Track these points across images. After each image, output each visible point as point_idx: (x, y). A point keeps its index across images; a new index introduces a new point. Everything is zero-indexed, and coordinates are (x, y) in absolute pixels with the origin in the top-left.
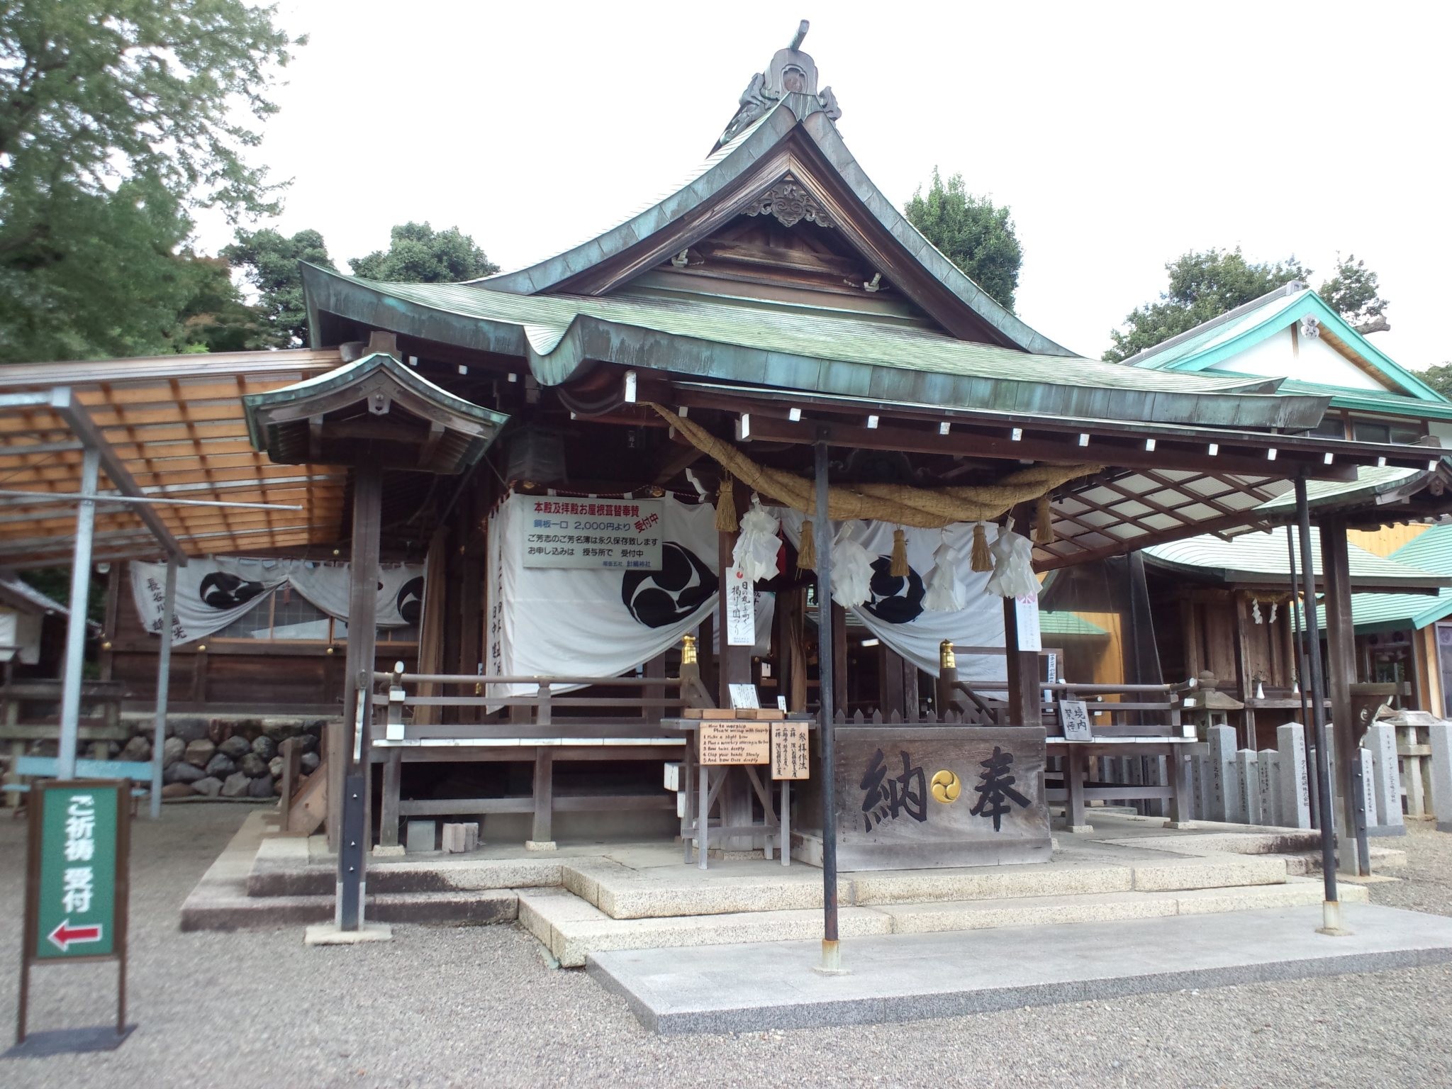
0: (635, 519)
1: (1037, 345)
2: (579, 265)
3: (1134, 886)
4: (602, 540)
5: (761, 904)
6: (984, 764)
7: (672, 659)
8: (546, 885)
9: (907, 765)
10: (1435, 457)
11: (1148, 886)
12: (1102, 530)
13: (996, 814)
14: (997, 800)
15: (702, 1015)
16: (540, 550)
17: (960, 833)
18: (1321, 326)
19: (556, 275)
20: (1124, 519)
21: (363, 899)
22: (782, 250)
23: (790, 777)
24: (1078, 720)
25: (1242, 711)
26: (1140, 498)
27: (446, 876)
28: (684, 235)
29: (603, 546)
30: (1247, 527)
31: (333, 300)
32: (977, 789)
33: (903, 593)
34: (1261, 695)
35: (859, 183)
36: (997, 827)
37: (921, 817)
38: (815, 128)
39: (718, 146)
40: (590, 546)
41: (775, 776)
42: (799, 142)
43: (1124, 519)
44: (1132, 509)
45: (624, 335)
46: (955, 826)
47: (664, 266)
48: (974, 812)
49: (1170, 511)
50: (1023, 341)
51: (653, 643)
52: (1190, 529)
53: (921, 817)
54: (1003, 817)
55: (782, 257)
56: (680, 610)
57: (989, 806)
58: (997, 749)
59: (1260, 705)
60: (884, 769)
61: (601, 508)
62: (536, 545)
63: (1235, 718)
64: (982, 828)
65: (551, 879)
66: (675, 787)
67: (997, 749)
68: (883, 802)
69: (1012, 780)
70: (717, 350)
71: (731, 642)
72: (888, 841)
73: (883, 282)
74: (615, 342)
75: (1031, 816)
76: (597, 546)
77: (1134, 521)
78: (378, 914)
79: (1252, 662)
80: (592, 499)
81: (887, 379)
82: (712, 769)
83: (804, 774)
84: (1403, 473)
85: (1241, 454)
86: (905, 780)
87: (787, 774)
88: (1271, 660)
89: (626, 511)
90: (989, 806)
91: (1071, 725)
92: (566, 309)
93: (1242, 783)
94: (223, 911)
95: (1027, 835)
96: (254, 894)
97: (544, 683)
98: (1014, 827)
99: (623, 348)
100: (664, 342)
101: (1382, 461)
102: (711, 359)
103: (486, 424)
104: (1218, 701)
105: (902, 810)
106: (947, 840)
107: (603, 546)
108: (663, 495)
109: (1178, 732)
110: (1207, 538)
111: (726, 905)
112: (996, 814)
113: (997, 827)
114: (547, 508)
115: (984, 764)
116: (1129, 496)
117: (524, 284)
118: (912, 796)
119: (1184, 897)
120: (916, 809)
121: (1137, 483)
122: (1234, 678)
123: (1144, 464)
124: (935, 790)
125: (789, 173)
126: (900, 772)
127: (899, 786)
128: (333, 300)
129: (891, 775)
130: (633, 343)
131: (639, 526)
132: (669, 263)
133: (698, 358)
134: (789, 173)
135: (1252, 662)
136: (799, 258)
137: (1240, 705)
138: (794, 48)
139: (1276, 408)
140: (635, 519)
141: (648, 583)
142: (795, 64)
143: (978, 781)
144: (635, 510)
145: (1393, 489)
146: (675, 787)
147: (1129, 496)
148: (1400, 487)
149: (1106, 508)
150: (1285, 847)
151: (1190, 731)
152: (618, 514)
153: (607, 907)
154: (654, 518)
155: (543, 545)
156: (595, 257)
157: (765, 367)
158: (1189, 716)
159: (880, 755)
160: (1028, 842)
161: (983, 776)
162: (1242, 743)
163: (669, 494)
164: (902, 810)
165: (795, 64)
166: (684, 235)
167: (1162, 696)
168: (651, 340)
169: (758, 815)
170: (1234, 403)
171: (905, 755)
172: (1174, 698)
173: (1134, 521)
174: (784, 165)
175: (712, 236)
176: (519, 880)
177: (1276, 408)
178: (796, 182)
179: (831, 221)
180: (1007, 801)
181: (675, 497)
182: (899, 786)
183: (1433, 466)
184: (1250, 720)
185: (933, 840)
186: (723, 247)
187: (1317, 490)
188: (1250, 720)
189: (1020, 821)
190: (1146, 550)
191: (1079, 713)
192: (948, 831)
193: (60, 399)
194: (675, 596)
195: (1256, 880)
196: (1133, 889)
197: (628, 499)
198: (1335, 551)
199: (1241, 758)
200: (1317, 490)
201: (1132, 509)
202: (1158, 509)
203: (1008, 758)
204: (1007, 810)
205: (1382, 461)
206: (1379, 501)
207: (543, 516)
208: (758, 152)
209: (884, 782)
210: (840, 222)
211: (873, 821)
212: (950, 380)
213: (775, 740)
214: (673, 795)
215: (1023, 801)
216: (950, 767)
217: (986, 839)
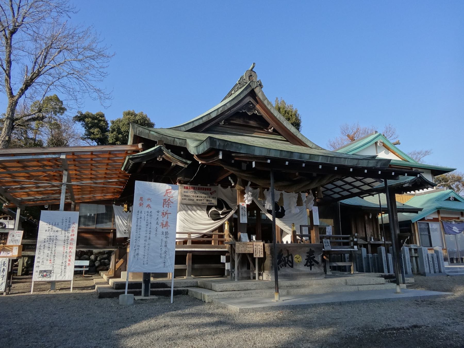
0: (210, 192)
1: (314, 146)
2: (197, 124)
3: (346, 283)
4: (201, 197)
5: (254, 288)
6: (307, 253)
7: (221, 228)
8: (193, 287)
9: (288, 254)
10: (419, 174)
11: (350, 284)
12: (329, 196)
13: (311, 266)
14: (311, 262)
15: (250, 309)
16: (185, 199)
17: (302, 271)
18: (383, 143)
19: (191, 126)
20: (335, 193)
21: (150, 289)
22: (248, 121)
23: (259, 257)
24: (327, 244)
25: (367, 244)
26: (340, 187)
27: (167, 284)
28: (223, 116)
29: (202, 199)
30: (368, 195)
31: (138, 132)
32: (306, 259)
33: (280, 211)
34: (373, 240)
35: (268, 105)
36: (311, 269)
37: (292, 267)
38: (257, 90)
39: (230, 94)
40: (198, 198)
41: (255, 256)
42: (252, 94)
43: (335, 193)
44: (338, 190)
45: (220, 142)
46: (301, 269)
47: (217, 124)
48: (305, 266)
49: (347, 190)
50: (310, 145)
51: (218, 224)
52: (353, 195)
53: (292, 267)
54: (312, 267)
55: (248, 123)
56: (222, 216)
57: (309, 264)
58: (311, 249)
59: (372, 242)
60: (283, 254)
61: (201, 188)
62: (184, 198)
63: (365, 246)
64: (307, 269)
65: (194, 285)
66: (225, 261)
67: (311, 249)
68: (283, 263)
69: (314, 257)
70: (243, 146)
71: (241, 222)
72: (283, 273)
73: (274, 130)
74: (218, 143)
75: (319, 266)
76: (200, 198)
77: (338, 193)
78: (153, 293)
79: (369, 231)
80: (199, 186)
81: (284, 154)
82: (239, 254)
83: (262, 256)
84: (412, 178)
85: (372, 173)
86: (288, 257)
87: (258, 256)
88: (373, 231)
89: (208, 189)
90: (309, 264)
91: (326, 246)
92: (204, 136)
93: (368, 263)
94: (110, 293)
95: (318, 272)
96: (116, 289)
97: (189, 234)
98: (315, 269)
99: (219, 145)
100: (230, 144)
101: (406, 174)
102: (241, 148)
103: (186, 163)
104: (361, 242)
105: (287, 265)
106: (298, 273)
107: (202, 199)
108: (218, 185)
109: (353, 248)
110: (357, 198)
111: (245, 288)
112: (311, 266)
113: (311, 269)
114: (187, 188)
115: (307, 253)
116: (337, 186)
117: (183, 129)
118: (290, 261)
119: (359, 286)
120: (291, 264)
121: (350, 179)
122: (364, 236)
123: (350, 174)
124: (295, 260)
125: (250, 101)
126: (286, 255)
127: (286, 259)
128: (138, 132)
129: (285, 255)
130: (222, 144)
131: (211, 193)
132: (219, 124)
133: (238, 148)
134: (250, 101)
135: (369, 231)
136: (252, 123)
137: (367, 243)
138: (252, 70)
139: (377, 162)
140: (210, 192)
141: (213, 209)
142: (251, 74)
143: (306, 257)
144: (210, 189)
145: (407, 183)
146: (225, 261)
147: (337, 186)
148: (410, 182)
149: (331, 190)
150: (382, 276)
151: (356, 247)
152: (206, 190)
153: (214, 289)
154: (215, 191)
155: (186, 198)
156: (201, 122)
157: (254, 150)
158: (356, 244)
159: (281, 251)
160: (319, 273)
161: (307, 256)
162: (368, 253)
163: (219, 185)
164: (287, 265)
165: (251, 74)
166: (223, 116)
167: (347, 238)
168: (226, 143)
169: (249, 268)
170: (367, 161)
171: (288, 251)
172: (351, 239)
173: (338, 193)
174: (249, 99)
175: (230, 117)
176: (186, 285)
177: (377, 162)
178: (252, 104)
179: (260, 114)
180: (313, 263)
181: (221, 186)
182: (286, 259)
183: (418, 176)
184: (369, 247)
185: (295, 272)
186: (233, 120)
187: (391, 182)
188: (369, 247)
189: (317, 268)
190: (341, 201)
191: (328, 242)
192: (299, 270)
193: (63, 157)
194: (220, 212)
195: (377, 283)
196: (346, 285)
197: (209, 186)
198: (391, 200)
199: (368, 256)
200: (391, 182)
201: (338, 190)
202: (344, 190)
203: (313, 252)
204: (313, 265)
205: (406, 174)
206: (404, 186)
207: (186, 190)
208: (242, 96)
209: (283, 258)
210: (263, 114)
211: (280, 268)
212: (299, 154)
213: (255, 247)
214: (224, 264)
215: (317, 263)
216: (299, 254)
217: (308, 272)
